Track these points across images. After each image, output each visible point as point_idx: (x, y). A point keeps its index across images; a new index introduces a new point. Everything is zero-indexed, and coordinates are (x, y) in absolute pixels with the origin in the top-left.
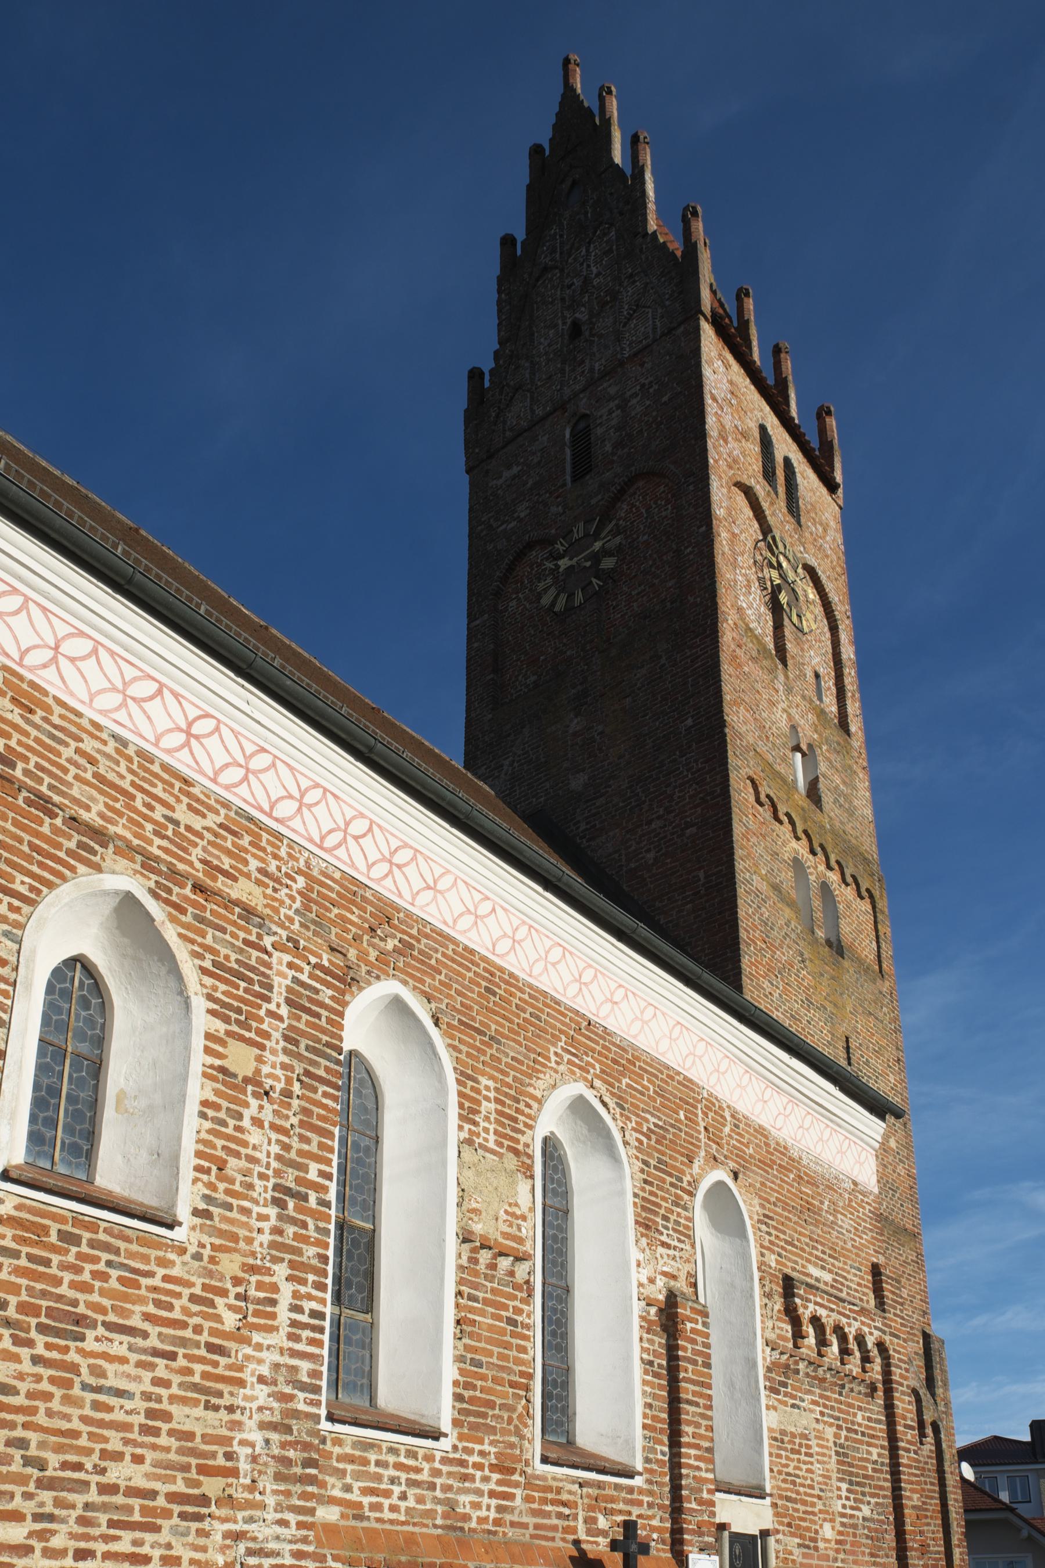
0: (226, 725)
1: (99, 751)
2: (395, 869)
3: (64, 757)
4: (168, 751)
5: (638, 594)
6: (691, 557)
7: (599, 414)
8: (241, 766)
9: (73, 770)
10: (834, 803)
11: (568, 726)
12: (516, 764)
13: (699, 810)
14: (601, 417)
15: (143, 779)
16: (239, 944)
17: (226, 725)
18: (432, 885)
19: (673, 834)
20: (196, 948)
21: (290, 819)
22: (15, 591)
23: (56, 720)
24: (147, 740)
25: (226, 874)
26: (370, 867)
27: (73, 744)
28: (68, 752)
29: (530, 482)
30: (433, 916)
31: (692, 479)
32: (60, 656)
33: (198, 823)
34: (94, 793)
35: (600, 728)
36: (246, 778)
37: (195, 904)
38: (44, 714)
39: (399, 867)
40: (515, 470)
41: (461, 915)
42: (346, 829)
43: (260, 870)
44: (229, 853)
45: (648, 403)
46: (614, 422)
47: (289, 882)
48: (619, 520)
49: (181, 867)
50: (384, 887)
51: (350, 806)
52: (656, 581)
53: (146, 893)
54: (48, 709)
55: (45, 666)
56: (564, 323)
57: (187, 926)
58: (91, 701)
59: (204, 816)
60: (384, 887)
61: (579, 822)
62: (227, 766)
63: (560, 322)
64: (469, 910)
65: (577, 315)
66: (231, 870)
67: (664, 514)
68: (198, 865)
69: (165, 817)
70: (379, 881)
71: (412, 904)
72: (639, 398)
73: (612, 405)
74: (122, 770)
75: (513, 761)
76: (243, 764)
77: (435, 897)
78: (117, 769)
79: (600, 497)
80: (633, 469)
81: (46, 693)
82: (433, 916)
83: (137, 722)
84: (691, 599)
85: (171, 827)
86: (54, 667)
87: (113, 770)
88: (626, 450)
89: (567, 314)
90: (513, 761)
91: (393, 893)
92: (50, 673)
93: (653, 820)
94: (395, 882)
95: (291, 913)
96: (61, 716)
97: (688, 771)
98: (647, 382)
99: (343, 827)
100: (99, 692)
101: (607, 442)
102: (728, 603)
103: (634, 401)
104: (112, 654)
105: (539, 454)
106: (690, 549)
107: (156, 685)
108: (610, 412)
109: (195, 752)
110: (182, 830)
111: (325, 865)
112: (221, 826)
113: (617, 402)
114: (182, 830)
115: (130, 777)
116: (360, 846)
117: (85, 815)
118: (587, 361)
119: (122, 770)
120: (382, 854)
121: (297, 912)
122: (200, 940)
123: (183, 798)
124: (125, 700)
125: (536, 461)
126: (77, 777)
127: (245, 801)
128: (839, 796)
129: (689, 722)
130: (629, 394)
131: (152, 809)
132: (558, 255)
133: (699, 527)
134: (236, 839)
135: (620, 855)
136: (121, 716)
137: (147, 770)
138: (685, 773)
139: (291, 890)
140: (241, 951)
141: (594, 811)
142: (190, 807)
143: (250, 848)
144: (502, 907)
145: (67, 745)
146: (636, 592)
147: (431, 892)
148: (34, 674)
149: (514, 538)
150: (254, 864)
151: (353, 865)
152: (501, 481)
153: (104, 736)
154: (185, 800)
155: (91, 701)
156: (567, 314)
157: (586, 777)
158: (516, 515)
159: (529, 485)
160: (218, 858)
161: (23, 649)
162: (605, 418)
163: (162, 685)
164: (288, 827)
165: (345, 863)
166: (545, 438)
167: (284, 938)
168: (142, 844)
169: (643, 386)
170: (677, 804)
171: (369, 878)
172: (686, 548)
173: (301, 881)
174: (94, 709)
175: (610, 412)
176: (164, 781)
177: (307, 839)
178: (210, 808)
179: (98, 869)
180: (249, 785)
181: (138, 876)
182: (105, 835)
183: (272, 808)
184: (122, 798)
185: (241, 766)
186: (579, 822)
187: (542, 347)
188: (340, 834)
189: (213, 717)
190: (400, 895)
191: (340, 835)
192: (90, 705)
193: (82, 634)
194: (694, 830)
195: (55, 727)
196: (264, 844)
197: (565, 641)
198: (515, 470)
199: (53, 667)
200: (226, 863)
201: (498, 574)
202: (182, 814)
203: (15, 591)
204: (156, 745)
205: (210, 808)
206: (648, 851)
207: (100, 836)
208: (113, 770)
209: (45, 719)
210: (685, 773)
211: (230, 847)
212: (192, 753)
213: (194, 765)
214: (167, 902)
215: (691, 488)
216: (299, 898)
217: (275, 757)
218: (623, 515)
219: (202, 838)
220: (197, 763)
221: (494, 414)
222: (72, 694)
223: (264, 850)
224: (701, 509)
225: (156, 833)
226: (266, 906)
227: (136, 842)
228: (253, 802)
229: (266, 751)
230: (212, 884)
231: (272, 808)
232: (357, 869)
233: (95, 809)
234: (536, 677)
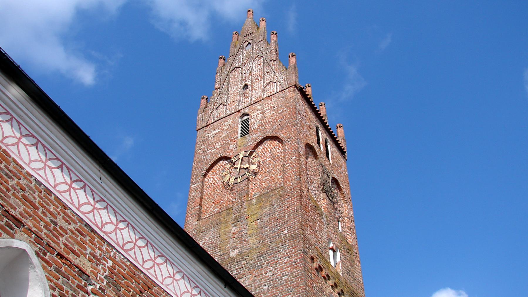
0: (89, 186)
1: (27, 185)
2: (156, 265)
3: (10, 184)
4: (60, 192)
5: (265, 180)
6: (289, 167)
7: (253, 115)
8: (92, 205)
9: (13, 191)
10: (347, 273)
11: (231, 230)
12: (206, 244)
13: (289, 268)
14: (254, 116)
15: (45, 202)
16: (75, 287)
17: (89, 186)
18: (172, 276)
19: (277, 278)
20: (53, 284)
21: (110, 233)
22: (8, 113)
23: (11, 167)
24: (51, 185)
25: (74, 252)
26: (144, 262)
27: (16, 180)
28: (13, 183)
29: (223, 136)
30: (171, 291)
31: (290, 140)
32: (20, 143)
33: (65, 225)
34: (20, 203)
35: (245, 232)
36: (92, 211)
37: (56, 262)
38: (6, 164)
39: (158, 264)
40: (217, 131)
41: (184, 292)
42: (136, 242)
43: (91, 254)
44: (78, 243)
45: (273, 112)
46: (259, 118)
47: (104, 262)
48: (259, 152)
49: (53, 244)
50: (149, 273)
51: (139, 232)
52: (273, 176)
53: (34, 253)
54: (9, 163)
55: (12, 145)
56: (241, 84)
57: (49, 272)
58: (29, 163)
59: (70, 224)
60: (149, 273)
61: (233, 270)
62: (85, 204)
63: (240, 84)
64: (188, 291)
65: (247, 82)
66: (77, 251)
67: (278, 151)
68: (63, 247)
69: (51, 220)
70: (147, 269)
71: (162, 283)
72: (269, 111)
73: (259, 112)
74: (36, 195)
75: (205, 242)
76: (93, 204)
77: (173, 282)
78: (34, 195)
79: (251, 143)
80: (266, 134)
81: (10, 156)
82: (171, 291)
83: (48, 176)
84: (288, 183)
85: (53, 225)
86: (16, 146)
87: (32, 195)
88: (263, 128)
89: (243, 82)
90: (205, 242)
91: (153, 276)
92: (14, 149)
93: (267, 272)
94: (155, 271)
95: (103, 277)
96: (14, 167)
97: (284, 252)
98: (273, 106)
99: (134, 241)
100: (34, 161)
101: (256, 124)
102: (304, 186)
103: (267, 112)
104: (44, 146)
105: (227, 126)
106: (288, 164)
107: (61, 163)
108: (258, 115)
109: (72, 194)
110: (58, 228)
111: (123, 257)
112: (76, 230)
113: (260, 111)
114: (58, 228)
115: (38, 199)
116: (141, 251)
117: (12, 212)
118: (250, 97)
119: (36, 195)
120: (151, 257)
121: (106, 277)
122: (55, 281)
123: (61, 214)
124: (45, 166)
125: (226, 128)
126: (13, 194)
127: (90, 221)
128: (349, 270)
129: (286, 231)
130: (265, 109)
131: (45, 215)
132: (241, 64)
133: (292, 157)
134: (83, 237)
135: (251, 286)
136: (42, 172)
137: (47, 198)
138: (283, 253)
139: (105, 266)
140: (75, 290)
141: (240, 266)
142: (64, 218)
143: (88, 242)
144: (204, 292)
145: (13, 180)
146: (265, 179)
147: (172, 279)
148: (7, 147)
149: (214, 155)
150: (89, 251)
151: (136, 260)
152: (210, 135)
153: (32, 179)
154: (62, 214)
155: (29, 163)
156: (243, 82)
157: (238, 251)
158: (215, 147)
159: (222, 137)
160: (72, 244)
161: (5, 136)
162: (255, 116)
163: (63, 163)
164: (109, 236)
165: (132, 258)
166: (231, 121)
167: (98, 287)
168: (36, 230)
169: (271, 107)
170: (279, 266)
171: (143, 267)
172: (287, 164)
173: (110, 263)
174: (30, 167)
175: (258, 115)
176: (54, 205)
177: (116, 244)
178: (73, 221)
179: (13, 237)
180: (94, 214)
181: (31, 244)
182: (21, 222)
183: (102, 227)
184: (32, 208)
185: (92, 205)
186: (233, 270)
187: (232, 91)
188: (133, 245)
189: (83, 182)
190: (157, 278)
191: (132, 245)
192: (28, 165)
193: (33, 136)
194: (287, 277)
195: (10, 171)
196: (96, 241)
197: (232, 196)
198: (217, 131)
199: (16, 146)
200: (76, 247)
201: (206, 168)
202: (60, 221)
203: (8, 113)
204: (54, 188)
205: (73, 221)
206: (265, 285)
207: (18, 222)
208: (32, 195)
209: (6, 166)
210: (283, 253)
211: (79, 240)
212: (70, 195)
213: (70, 200)
214: (43, 259)
215: (290, 142)
216: (108, 270)
217: (108, 204)
218: (260, 150)
219: (67, 234)
220: (72, 200)
221: (210, 112)
222: (21, 159)
223: (95, 245)
224: (293, 151)
225: (45, 227)
226: (92, 271)
227: (34, 229)
228: (94, 222)
229: (105, 201)
230: (67, 256)
231: (102, 227)
232: (138, 262)
233: (18, 210)
234: (218, 209)
